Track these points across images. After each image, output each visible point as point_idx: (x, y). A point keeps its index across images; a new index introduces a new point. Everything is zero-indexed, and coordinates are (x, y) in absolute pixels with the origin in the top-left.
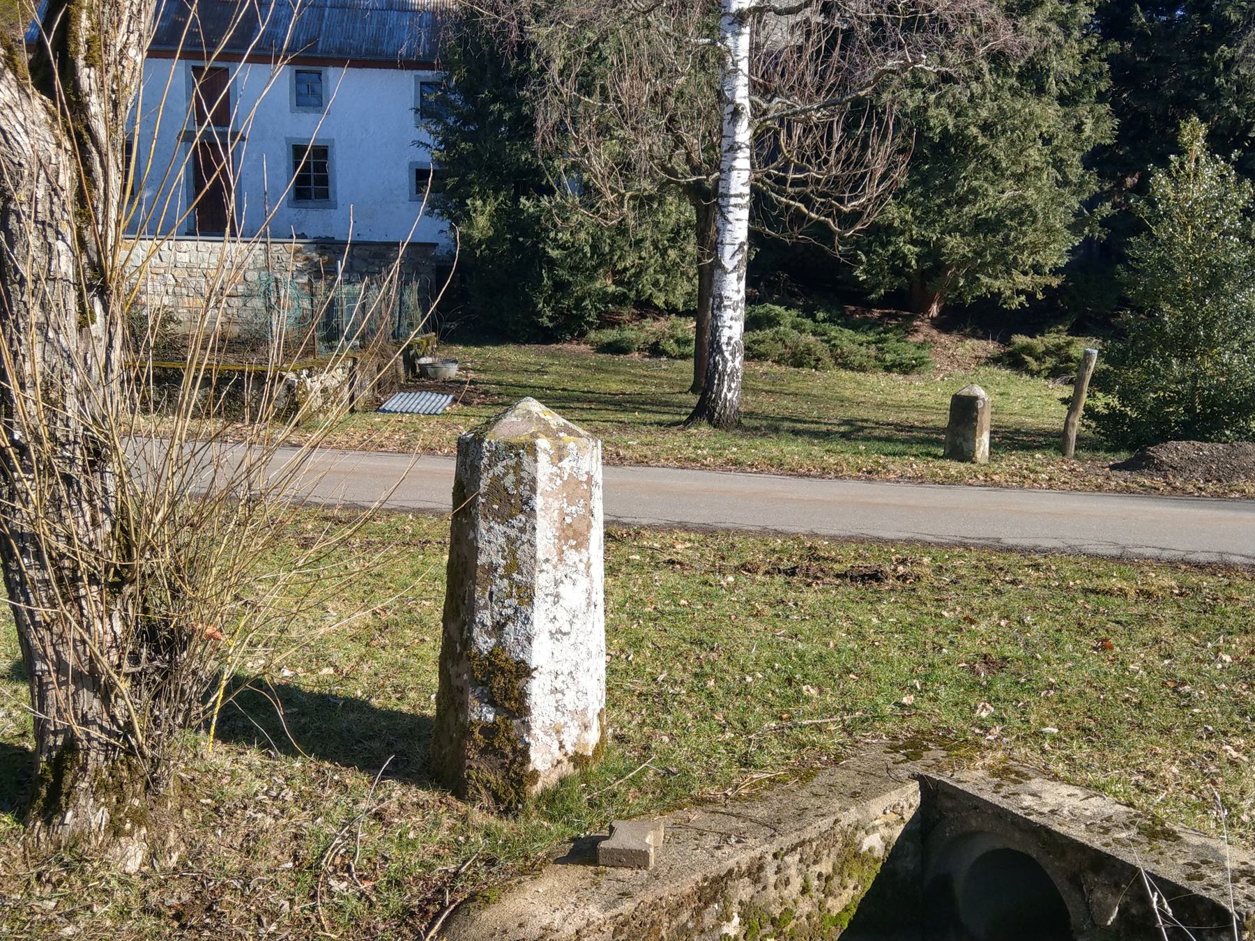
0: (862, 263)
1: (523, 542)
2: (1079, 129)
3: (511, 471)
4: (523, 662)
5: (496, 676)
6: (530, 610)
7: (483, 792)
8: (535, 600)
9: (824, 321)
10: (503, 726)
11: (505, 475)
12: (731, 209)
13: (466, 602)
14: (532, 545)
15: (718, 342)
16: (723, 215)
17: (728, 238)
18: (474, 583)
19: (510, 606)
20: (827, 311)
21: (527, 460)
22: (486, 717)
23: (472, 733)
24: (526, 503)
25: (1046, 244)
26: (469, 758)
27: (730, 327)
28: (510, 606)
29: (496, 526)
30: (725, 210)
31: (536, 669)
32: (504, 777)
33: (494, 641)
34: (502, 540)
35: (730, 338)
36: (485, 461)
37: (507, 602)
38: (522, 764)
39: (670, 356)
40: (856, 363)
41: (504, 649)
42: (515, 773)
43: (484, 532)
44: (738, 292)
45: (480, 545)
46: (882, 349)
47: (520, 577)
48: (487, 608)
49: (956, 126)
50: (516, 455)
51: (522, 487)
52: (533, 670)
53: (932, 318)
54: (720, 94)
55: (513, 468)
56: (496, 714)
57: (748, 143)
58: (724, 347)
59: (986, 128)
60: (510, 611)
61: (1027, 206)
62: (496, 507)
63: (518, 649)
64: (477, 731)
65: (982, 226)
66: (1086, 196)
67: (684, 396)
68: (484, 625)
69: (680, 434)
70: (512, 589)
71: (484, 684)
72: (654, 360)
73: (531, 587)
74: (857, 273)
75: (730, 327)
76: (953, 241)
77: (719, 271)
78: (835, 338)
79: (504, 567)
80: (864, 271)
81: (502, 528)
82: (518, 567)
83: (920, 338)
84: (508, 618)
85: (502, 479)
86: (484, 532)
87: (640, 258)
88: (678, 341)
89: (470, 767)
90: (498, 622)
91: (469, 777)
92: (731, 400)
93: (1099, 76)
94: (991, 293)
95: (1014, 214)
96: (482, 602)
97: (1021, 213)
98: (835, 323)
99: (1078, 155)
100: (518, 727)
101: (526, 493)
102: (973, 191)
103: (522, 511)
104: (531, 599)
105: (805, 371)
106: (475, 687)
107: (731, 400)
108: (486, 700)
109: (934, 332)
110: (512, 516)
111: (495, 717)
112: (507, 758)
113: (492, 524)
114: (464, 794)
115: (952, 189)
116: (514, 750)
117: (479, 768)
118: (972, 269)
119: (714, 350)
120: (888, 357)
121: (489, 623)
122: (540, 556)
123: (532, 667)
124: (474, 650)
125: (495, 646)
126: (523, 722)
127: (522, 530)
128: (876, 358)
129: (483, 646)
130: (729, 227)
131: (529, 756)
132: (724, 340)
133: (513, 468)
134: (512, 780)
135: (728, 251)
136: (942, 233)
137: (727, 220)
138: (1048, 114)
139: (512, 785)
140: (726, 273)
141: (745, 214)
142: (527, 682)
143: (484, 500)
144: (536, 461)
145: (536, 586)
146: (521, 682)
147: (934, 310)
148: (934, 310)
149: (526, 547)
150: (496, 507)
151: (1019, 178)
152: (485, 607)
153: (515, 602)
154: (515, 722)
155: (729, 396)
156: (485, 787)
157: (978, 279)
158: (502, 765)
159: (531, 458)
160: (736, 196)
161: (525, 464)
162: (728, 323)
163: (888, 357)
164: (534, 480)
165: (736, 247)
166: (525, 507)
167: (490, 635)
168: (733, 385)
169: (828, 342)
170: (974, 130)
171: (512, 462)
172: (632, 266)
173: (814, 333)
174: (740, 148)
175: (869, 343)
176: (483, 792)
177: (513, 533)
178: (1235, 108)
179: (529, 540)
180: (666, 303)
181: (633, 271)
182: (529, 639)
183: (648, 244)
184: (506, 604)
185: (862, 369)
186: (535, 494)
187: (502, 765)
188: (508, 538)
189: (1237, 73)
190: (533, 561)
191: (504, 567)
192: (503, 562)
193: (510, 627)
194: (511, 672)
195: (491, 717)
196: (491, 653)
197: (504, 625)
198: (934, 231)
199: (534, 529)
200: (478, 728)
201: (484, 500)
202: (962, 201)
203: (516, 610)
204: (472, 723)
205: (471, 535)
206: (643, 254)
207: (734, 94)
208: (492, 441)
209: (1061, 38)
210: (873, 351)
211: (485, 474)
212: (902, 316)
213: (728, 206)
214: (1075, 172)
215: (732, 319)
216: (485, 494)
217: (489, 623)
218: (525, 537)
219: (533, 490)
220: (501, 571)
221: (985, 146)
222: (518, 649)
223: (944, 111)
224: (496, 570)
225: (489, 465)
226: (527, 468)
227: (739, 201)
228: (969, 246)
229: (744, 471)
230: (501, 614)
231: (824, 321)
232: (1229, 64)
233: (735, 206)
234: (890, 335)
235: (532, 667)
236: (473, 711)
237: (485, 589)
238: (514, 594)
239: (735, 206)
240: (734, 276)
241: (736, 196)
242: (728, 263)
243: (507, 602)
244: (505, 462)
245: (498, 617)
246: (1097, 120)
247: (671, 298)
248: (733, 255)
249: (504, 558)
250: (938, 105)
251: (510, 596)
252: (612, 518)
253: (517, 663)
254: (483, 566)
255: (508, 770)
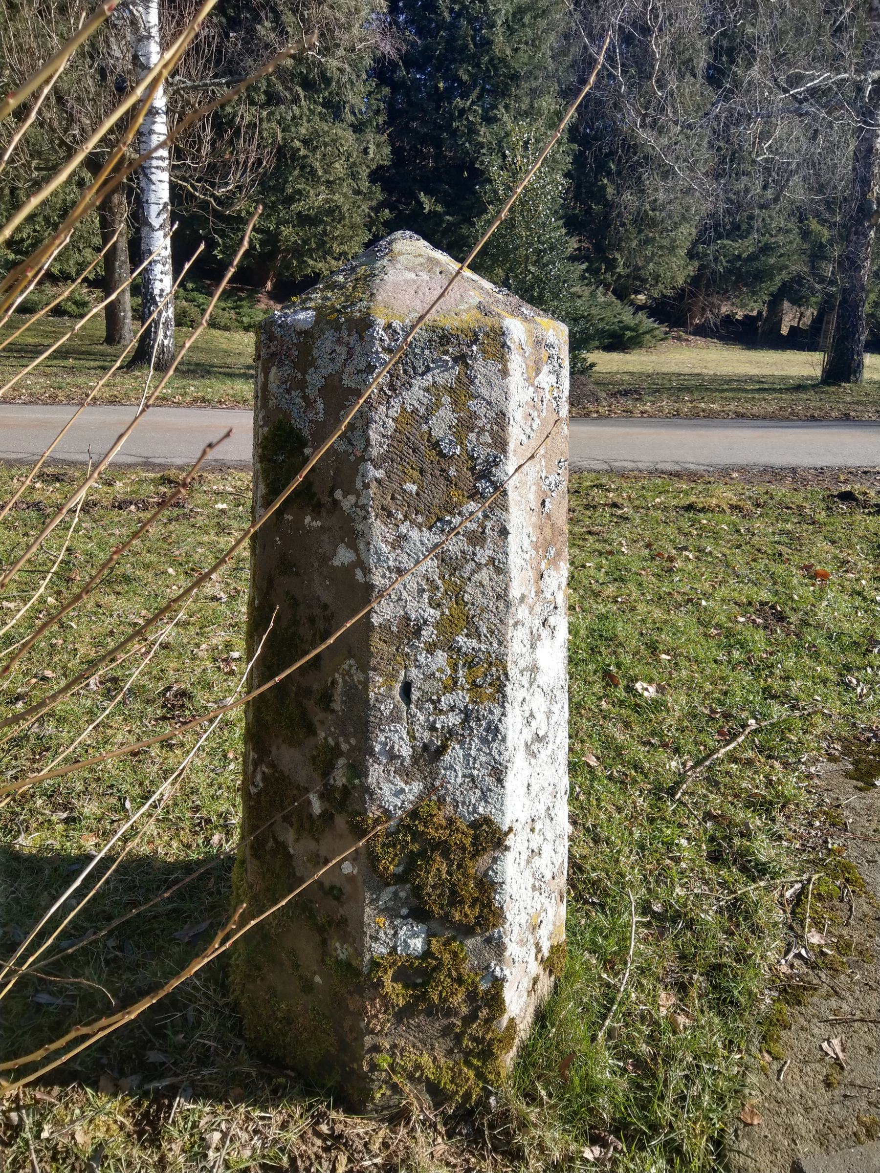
0: (219, 245)
1: (479, 565)
2: (365, 151)
3: (446, 399)
4: (487, 821)
5: (428, 860)
6: (497, 712)
7: (408, 1087)
8: (508, 690)
9: (192, 290)
10: (446, 957)
11: (431, 409)
12: (153, 170)
13: (337, 706)
14: (499, 571)
15: (152, 293)
16: (146, 175)
17: (153, 198)
18: (364, 667)
19: (452, 708)
20: (194, 282)
21: (482, 368)
22: (407, 945)
23: (380, 984)
24: (486, 475)
25: (352, 237)
26: (372, 1032)
27: (161, 281)
28: (452, 708)
29: (414, 534)
30: (148, 171)
31: (511, 829)
32: (450, 1052)
33: (417, 787)
34: (430, 566)
35: (162, 290)
36: (380, 377)
37: (446, 701)
38: (488, 1021)
39: (71, 316)
40: (222, 324)
41: (441, 801)
42: (474, 1039)
43: (385, 548)
44: (166, 248)
45: (378, 580)
46: (239, 314)
47: (474, 643)
48: (399, 720)
49: (284, 139)
50: (455, 360)
51: (473, 436)
52: (507, 834)
53: (268, 292)
54: (136, 57)
55: (451, 391)
56: (430, 935)
57: (164, 109)
58: (158, 298)
59: (306, 142)
60: (454, 720)
61: (338, 207)
62: (411, 488)
63: (473, 797)
64: (387, 979)
65: (303, 220)
66: (374, 203)
67: (101, 347)
68: (392, 756)
69: (126, 376)
70: (456, 671)
71: (400, 879)
72: (58, 319)
73: (500, 662)
74: (216, 252)
75: (161, 281)
76: (286, 231)
77: (147, 229)
78: (203, 304)
79: (437, 625)
80: (221, 252)
81: (430, 538)
82: (469, 620)
83: (262, 306)
84: (450, 734)
85: (426, 420)
86: (385, 548)
87: (35, 231)
88: (76, 303)
89: (376, 1049)
90: (425, 747)
91: (374, 1067)
92: (168, 346)
93: (378, 112)
94: (315, 273)
95: (330, 212)
96: (386, 708)
97: (333, 212)
98: (201, 293)
99: (368, 170)
100: (478, 953)
101: (482, 453)
102: (299, 192)
103: (475, 494)
104: (500, 689)
105: (184, 329)
106: (378, 889)
107: (168, 346)
108: (404, 911)
109: (272, 303)
110: (450, 508)
111: (428, 942)
112: (457, 1014)
113: (403, 529)
114: (363, 1103)
115: (283, 190)
116: (472, 996)
117: (394, 1046)
118: (298, 252)
119: (148, 301)
120: (246, 320)
121: (406, 751)
122: (515, 592)
123: (505, 828)
124: (373, 812)
125: (420, 798)
126: (488, 941)
127: (477, 539)
128: (236, 320)
129: (392, 801)
130: (153, 187)
131: (503, 1002)
132: (157, 292)
133: (451, 391)
134: (468, 1053)
135: (154, 210)
136: (277, 224)
137: (151, 180)
138: (348, 138)
139: (468, 1064)
140: (153, 230)
141: (165, 176)
142: (495, 860)
143: (380, 474)
144: (505, 373)
145: (509, 659)
146: (483, 861)
147: (269, 286)
148: (269, 286)
149: (484, 575)
150: (411, 488)
151: (329, 183)
152: (395, 717)
153: (462, 698)
154: (470, 943)
155: (166, 342)
156: (411, 1077)
157: (306, 262)
158: (446, 1031)
159: (494, 366)
160: (157, 158)
161: (479, 380)
162: (159, 277)
163: (246, 320)
164: (501, 419)
165: (161, 207)
166: (481, 485)
167: (407, 775)
168: (168, 333)
169: (199, 306)
170: (297, 144)
171: (445, 378)
172: (28, 238)
173: (187, 300)
174: (158, 113)
175: (230, 308)
176: (408, 1087)
177: (455, 546)
178: (467, 145)
179: (492, 560)
180: (60, 271)
181: (29, 241)
182: (498, 773)
183: (40, 219)
184: (443, 706)
185: (226, 328)
186: (504, 451)
187: (446, 1031)
188: (443, 559)
189: (467, 118)
190: (502, 606)
191: (437, 625)
192: (432, 614)
193: (455, 753)
194: (464, 849)
195: (417, 944)
196: (414, 814)
197: (441, 751)
198: (271, 222)
199: (504, 532)
200: (390, 973)
201: (380, 474)
202: (289, 200)
203: (467, 715)
204: (375, 964)
205: (344, 556)
206: (37, 228)
207: (148, 59)
208: (397, 324)
209: (354, 77)
210: (232, 314)
211: (382, 409)
212: (247, 290)
213: (151, 167)
214: (365, 185)
215: (162, 273)
216: (383, 458)
217: (406, 751)
218: (483, 555)
219: (501, 444)
220: (428, 633)
221: (305, 157)
222: (473, 797)
223: (274, 125)
224: (417, 633)
225: (392, 387)
226: (484, 391)
227: (160, 163)
228: (298, 235)
229: (214, 407)
230: (432, 728)
231: (192, 290)
232: (462, 112)
233: (157, 168)
234: (244, 303)
235: (505, 828)
236: (376, 939)
237: (393, 677)
238: (462, 680)
239: (157, 168)
240: (161, 233)
241: (157, 158)
242: (156, 222)
243: (446, 701)
244: (429, 377)
245: (426, 734)
246: (378, 146)
247: (66, 267)
248: (159, 214)
249: (436, 605)
250: (269, 120)
251: (452, 686)
252: (141, 459)
253: (474, 825)
254: (385, 627)
255: (458, 1038)
